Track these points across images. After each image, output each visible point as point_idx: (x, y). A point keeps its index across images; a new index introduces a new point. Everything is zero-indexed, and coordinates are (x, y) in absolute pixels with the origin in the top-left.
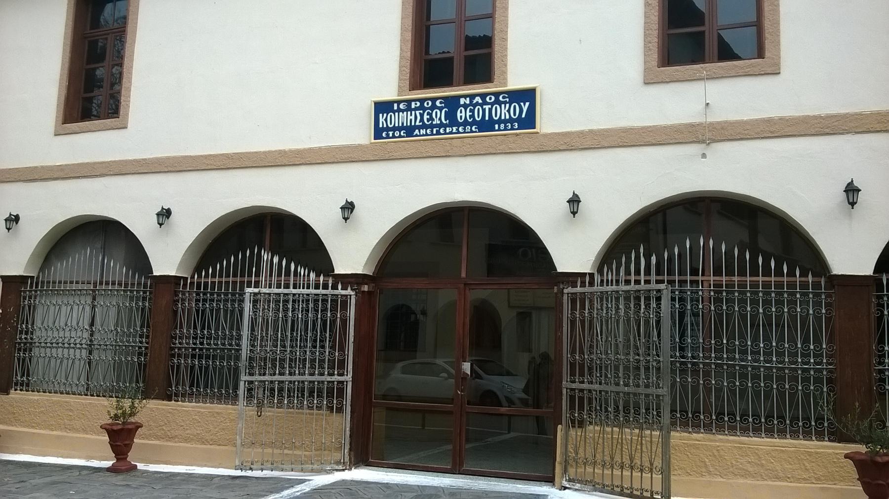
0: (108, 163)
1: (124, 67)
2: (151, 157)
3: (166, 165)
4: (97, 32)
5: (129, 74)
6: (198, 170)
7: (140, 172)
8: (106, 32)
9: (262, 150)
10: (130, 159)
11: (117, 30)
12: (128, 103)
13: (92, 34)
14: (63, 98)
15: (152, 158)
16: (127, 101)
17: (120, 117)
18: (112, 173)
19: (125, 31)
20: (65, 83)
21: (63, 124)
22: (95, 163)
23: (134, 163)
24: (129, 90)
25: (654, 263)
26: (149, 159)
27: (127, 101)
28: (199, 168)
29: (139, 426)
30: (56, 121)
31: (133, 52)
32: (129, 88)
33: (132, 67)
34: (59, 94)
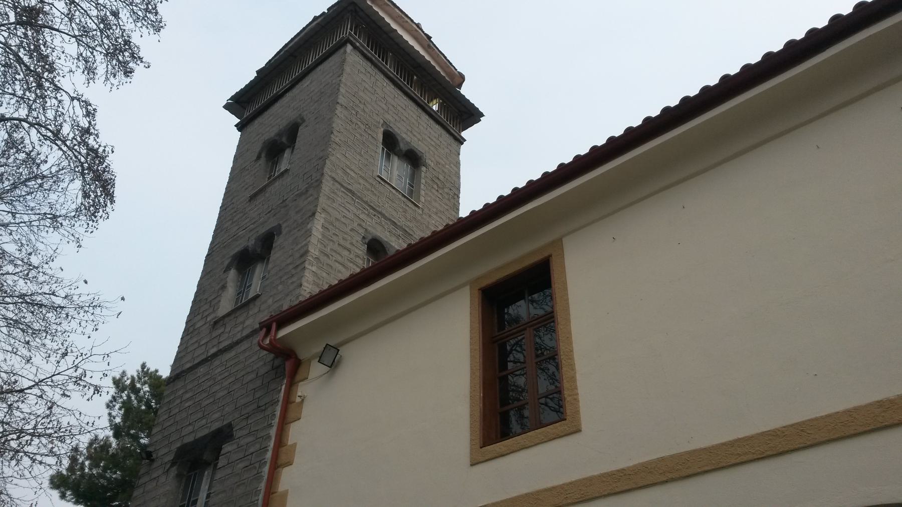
0: (562, 487)
1: (562, 353)
2: (631, 464)
3: (661, 471)
4: (502, 334)
5: (569, 361)
6: (723, 468)
7: (617, 490)
8: (518, 329)
9: (841, 407)
10: (596, 474)
11: (541, 319)
12: (575, 397)
13: (511, 332)
14: (478, 415)
15: (635, 466)
16: (573, 395)
17: (568, 418)
18: (569, 501)
19: (553, 317)
20: (479, 394)
21: (481, 448)
22: (538, 492)
23: (604, 479)
24: (573, 379)
25: (205, 479)
26: (628, 468)
27: (573, 395)
28: (725, 465)
29: (287, 491)
30: (472, 445)
31: (570, 333)
32: (573, 377)
33: (572, 351)
34: (471, 411)
